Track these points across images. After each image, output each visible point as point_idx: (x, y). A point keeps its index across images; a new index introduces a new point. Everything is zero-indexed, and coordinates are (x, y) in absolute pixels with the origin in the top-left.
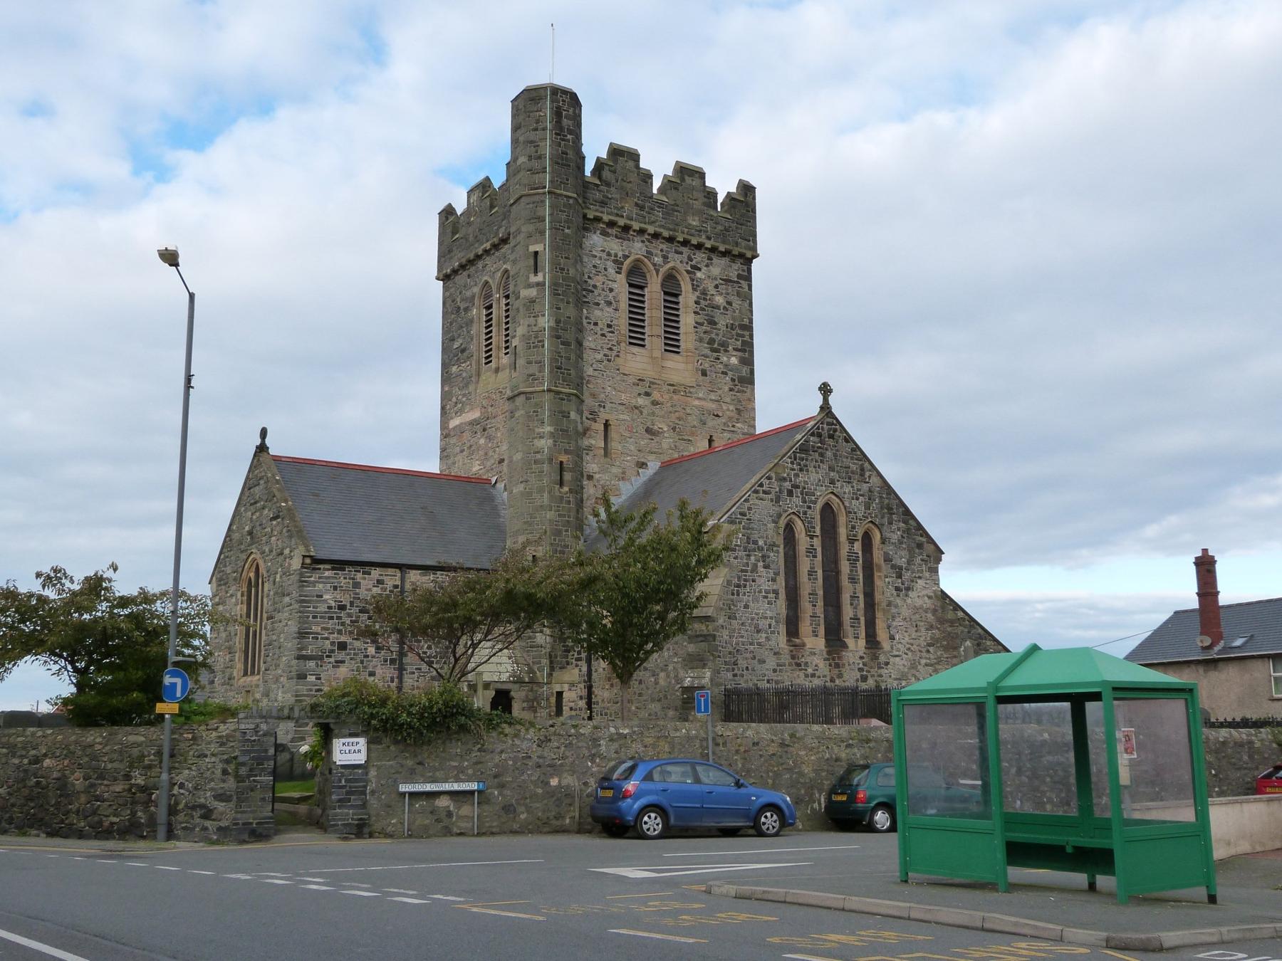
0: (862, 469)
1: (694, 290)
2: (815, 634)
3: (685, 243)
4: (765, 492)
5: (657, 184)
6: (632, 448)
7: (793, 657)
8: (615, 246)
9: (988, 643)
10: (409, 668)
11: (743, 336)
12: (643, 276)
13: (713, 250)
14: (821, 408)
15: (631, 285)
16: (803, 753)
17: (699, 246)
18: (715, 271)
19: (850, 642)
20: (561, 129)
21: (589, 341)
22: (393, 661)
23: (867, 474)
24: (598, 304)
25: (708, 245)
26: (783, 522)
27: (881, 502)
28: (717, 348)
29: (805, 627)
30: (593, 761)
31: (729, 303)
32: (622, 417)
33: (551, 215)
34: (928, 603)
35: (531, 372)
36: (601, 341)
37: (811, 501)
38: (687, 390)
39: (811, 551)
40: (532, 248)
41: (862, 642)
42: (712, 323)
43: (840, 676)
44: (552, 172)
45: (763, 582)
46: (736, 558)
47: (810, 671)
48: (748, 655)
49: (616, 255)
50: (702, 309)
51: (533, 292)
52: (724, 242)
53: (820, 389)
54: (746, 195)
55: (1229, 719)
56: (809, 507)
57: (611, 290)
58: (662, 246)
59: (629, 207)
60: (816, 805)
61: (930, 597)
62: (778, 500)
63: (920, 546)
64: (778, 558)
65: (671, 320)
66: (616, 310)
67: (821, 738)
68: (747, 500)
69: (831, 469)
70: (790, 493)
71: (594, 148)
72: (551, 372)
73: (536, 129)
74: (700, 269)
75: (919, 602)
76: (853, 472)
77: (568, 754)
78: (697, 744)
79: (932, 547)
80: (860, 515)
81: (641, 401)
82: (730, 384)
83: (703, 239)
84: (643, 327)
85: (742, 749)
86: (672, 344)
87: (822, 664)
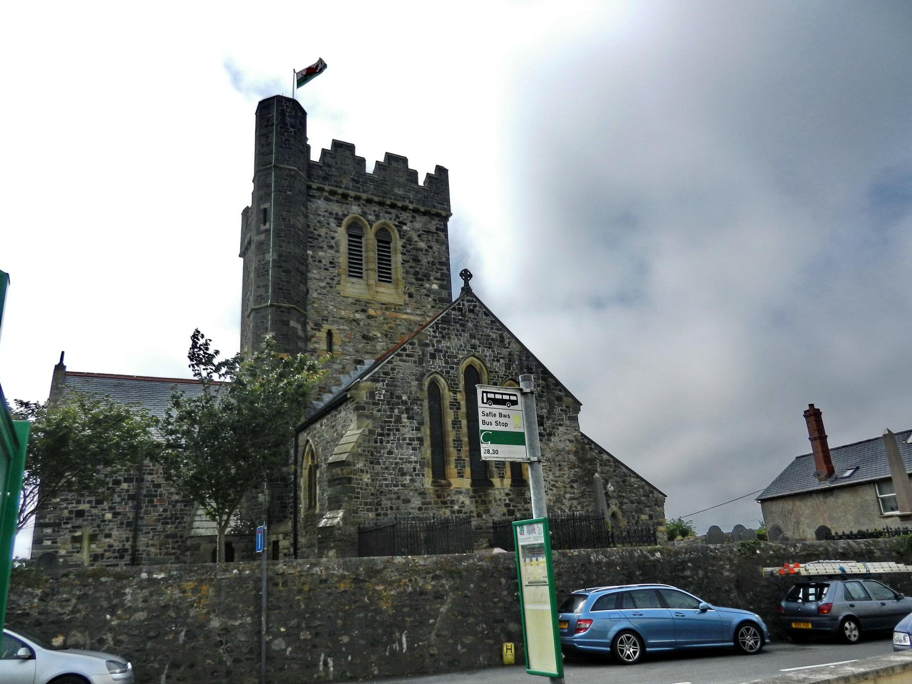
0: (502, 337)
1: (401, 238)
2: (461, 475)
3: (393, 206)
4: (407, 355)
5: (370, 168)
6: (351, 349)
7: (439, 497)
8: (336, 208)
9: (633, 480)
10: (145, 529)
11: (442, 270)
12: (361, 229)
13: (416, 211)
14: (462, 289)
15: (350, 236)
16: (381, 588)
17: (404, 208)
18: (418, 225)
19: (496, 481)
20: (285, 124)
21: (314, 273)
22: (129, 524)
23: (507, 341)
24: (322, 248)
25: (411, 207)
26: (426, 382)
27: (521, 364)
28: (421, 278)
29: (452, 469)
30: (113, 614)
31: (431, 247)
32: (342, 327)
33: (276, 182)
34: (571, 447)
35: (259, 293)
36: (324, 273)
37: (454, 363)
38: (397, 308)
39: (455, 405)
40: (262, 207)
41: (508, 482)
42: (416, 260)
43: (487, 511)
44: (277, 153)
45: (408, 431)
46: (379, 411)
47: (456, 507)
48: (393, 496)
49: (337, 214)
50: (408, 251)
51: (263, 237)
52: (424, 206)
53: (461, 275)
54: (440, 175)
55: (847, 532)
56: (453, 368)
57: (333, 238)
58: (374, 208)
59: (346, 181)
60: (396, 646)
61: (571, 441)
62: (421, 361)
63: (559, 399)
64: (424, 410)
65: (384, 261)
66: (337, 251)
67: (403, 570)
68: (389, 362)
69: (472, 336)
70: (433, 356)
71: (318, 141)
72: (273, 292)
73: (267, 126)
74: (405, 224)
75: (561, 446)
76: (493, 339)
77: (80, 607)
78: (251, 584)
79: (570, 399)
80: (501, 374)
81: (358, 316)
82: (433, 304)
83: (407, 203)
84: (361, 264)
85: (306, 588)
86: (385, 275)
87: (467, 501)
